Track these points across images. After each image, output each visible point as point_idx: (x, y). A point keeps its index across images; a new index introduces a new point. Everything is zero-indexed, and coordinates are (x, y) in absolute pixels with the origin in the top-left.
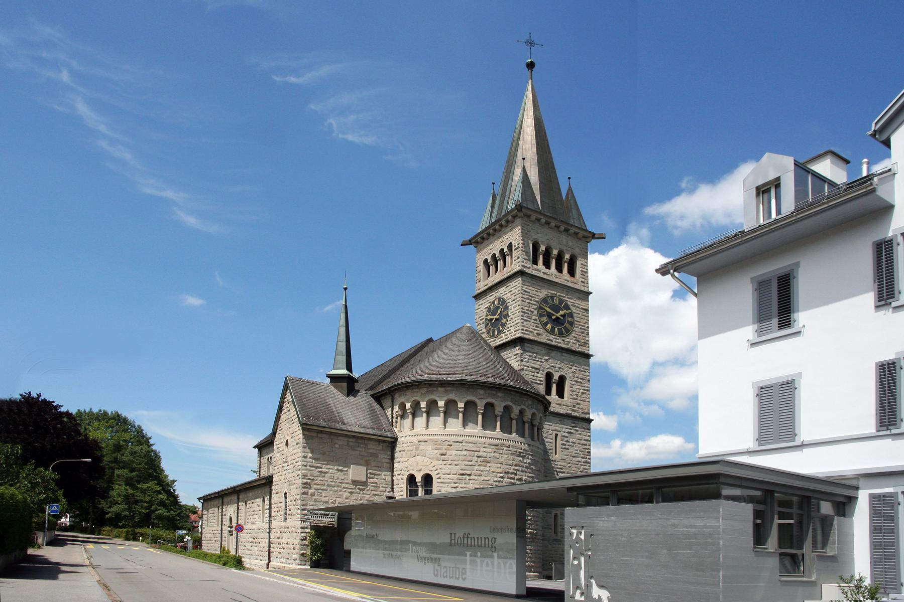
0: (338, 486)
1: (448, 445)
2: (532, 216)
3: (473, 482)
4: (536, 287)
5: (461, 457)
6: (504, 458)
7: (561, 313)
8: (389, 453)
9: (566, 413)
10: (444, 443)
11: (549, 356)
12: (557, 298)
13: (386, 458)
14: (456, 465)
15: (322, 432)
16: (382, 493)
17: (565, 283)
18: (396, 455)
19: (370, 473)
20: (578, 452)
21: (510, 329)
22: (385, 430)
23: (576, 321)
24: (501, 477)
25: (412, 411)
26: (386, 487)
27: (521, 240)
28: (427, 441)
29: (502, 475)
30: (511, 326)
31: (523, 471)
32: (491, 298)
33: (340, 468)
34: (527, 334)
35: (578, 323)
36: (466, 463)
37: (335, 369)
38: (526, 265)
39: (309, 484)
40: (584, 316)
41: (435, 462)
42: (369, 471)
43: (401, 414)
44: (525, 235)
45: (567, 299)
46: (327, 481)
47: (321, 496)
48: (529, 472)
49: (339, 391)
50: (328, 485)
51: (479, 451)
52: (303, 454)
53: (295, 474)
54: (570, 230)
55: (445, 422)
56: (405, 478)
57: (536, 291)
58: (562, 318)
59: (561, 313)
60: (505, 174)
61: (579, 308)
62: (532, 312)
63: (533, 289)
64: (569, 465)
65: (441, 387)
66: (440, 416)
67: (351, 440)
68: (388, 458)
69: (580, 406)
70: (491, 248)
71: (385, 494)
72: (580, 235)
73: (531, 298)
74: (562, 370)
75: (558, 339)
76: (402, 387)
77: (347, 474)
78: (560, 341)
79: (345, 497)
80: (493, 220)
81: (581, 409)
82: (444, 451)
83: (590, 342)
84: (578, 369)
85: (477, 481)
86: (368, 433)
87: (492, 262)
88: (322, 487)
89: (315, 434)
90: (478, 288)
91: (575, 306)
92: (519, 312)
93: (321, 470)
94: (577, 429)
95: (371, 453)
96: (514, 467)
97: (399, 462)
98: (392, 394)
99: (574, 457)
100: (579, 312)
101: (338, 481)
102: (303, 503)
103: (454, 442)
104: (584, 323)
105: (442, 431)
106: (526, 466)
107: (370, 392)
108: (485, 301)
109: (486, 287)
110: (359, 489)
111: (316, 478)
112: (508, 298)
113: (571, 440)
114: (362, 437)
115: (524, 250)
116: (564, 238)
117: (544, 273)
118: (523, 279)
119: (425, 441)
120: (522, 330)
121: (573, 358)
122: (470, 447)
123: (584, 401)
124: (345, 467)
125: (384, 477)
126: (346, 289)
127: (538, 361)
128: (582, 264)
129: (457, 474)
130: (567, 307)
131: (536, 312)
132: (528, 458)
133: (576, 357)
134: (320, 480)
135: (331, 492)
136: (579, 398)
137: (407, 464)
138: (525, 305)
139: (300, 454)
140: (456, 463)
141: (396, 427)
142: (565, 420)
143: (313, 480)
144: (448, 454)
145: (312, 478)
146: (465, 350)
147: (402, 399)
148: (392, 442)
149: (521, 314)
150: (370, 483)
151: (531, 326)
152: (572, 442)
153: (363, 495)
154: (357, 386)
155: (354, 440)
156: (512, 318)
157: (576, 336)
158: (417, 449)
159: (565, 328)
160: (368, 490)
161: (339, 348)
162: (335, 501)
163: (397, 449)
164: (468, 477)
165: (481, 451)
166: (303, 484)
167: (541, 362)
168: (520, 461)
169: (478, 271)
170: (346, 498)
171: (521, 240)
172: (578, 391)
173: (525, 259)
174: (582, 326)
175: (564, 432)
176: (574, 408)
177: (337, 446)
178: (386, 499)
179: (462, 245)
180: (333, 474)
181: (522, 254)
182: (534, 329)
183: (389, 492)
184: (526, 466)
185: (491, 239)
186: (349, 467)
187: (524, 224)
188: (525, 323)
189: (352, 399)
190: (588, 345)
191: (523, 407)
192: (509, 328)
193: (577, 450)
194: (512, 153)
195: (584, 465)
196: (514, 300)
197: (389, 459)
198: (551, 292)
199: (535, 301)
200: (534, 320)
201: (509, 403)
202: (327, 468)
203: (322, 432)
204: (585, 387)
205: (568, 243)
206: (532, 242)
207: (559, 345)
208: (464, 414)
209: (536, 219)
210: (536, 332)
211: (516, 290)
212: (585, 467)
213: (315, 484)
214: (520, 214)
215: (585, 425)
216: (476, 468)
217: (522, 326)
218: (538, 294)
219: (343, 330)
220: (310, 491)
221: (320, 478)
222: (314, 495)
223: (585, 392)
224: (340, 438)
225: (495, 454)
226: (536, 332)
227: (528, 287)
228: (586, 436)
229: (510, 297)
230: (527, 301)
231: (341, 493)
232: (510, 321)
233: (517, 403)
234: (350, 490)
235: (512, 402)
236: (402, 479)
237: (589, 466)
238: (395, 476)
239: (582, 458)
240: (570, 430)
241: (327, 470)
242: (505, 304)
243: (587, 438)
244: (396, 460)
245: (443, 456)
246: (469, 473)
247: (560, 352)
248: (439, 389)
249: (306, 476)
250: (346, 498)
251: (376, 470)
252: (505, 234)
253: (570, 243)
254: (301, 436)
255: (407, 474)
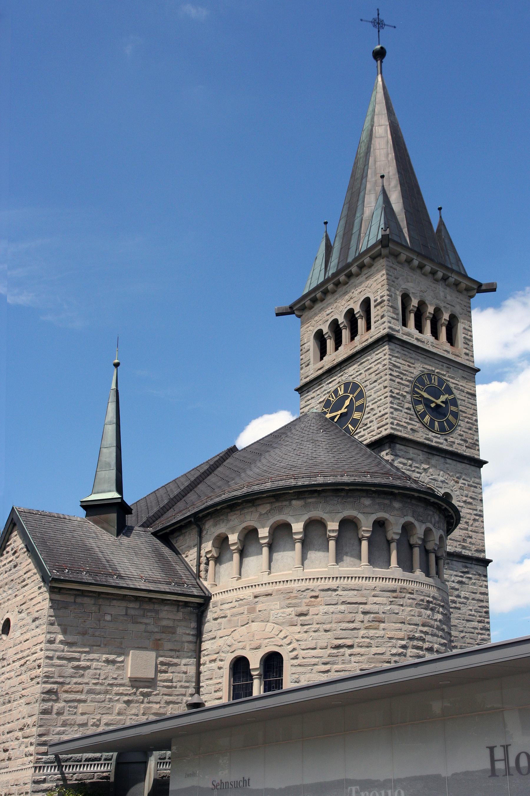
0: (106, 692)
1: (311, 597)
2: (402, 254)
3: (357, 658)
4: (408, 360)
5: (334, 616)
6: (406, 612)
7: (443, 398)
8: (194, 625)
9: (455, 552)
10: (304, 593)
11: (428, 464)
12: (436, 377)
13: (189, 634)
14: (326, 631)
15: (83, 593)
16: (180, 697)
17: (445, 355)
18: (207, 627)
19: (162, 664)
20: (473, 613)
21: (368, 426)
22: (188, 585)
23: (461, 411)
24: (404, 647)
25: (240, 547)
26: (187, 687)
27: (387, 290)
28: (271, 595)
29: (404, 643)
30: (371, 422)
31: (433, 635)
32: (330, 385)
33: (112, 657)
34: (398, 430)
35: (464, 415)
36: (345, 625)
37: (94, 493)
38: (394, 327)
39: (56, 693)
40: (470, 403)
41: (287, 630)
42: (161, 659)
43: (216, 555)
44: (391, 283)
45: (448, 379)
46: (87, 684)
47: (75, 713)
48: (441, 637)
49: (102, 528)
50: (90, 692)
51: (365, 604)
52: (49, 636)
53: (24, 677)
54: (450, 278)
55: (304, 558)
56: (226, 665)
57: (409, 366)
58: (444, 405)
59: (443, 398)
60: (346, 206)
61: (463, 392)
62: (404, 396)
63: (404, 362)
64: (462, 635)
65: (298, 499)
66: (293, 549)
67: (131, 605)
68: (192, 633)
69: (473, 540)
70: (328, 312)
71: (185, 699)
72: (463, 286)
73: (402, 376)
74: (446, 485)
75: (439, 438)
76: (221, 509)
77: (122, 668)
78: (441, 441)
79: (117, 711)
80: (332, 270)
81: (473, 544)
82: (303, 609)
83: (481, 443)
84: (466, 483)
85: (363, 657)
86: (163, 590)
87: (330, 334)
88: (78, 697)
89: (71, 599)
90: (305, 375)
91: (458, 389)
92: (386, 397)
93: (77, 663)
94: (470, 576)
95: (164, 626)
96: (421, 628)
97: (214, 638)
98: (199, 523)
99: (468, 621)
100: (464, 398)
101: (107, 682)
102: (42, 730)
103: (323, 590)
104: (471, 415)
105: (299, 574)
106: (437, 625)
107: (151, 529)
108: (318, 392)
109: (320, 372)
110: (142, 694)
111: (68, 680)
112: (365, 379)
113: (463, 594)
114: (151, 599)
115: (390, 304)
116: (441, 290)
117: (417, 339)
118: (391, 347)
119: (267, 595)
120: (392, 423)
121: (460, 466)
122: (351, 596)
123: (477, 532)
124: (119, 655)
125: (184, 668)
126: (117, 365)
127: (414, 471)
128: (464, 328)
129: (329, 647)
130: (449, 391)
131: (409, 397)
132: (438, 612)
133: (464, 465)
134: (76, 683)
135: (94, 704)
136: (470, 528)
137: (229, 640)
138: (395, 386)
139: (42, 638)
140: (327, 627)
141: (206, 579)
142: (454, 563)
143: (62, 684)
144: (311, 613)
145: (61, 680)
146: (324, 443)
147: (221, 529)
148: (200, 605)
149: (389, 399)
150: (161, 681)
151: (402, 417)
152: (465, 598)
153: (148, 705)
154: (130, 520)
155: (136, 605)
156: (372, 409)
157: (462, 433)
158: (251, 610)
159: (448, 421)
160: (156, 695)
161: (103, 459)
162: (99, 720)
163: (210, 615)
164: (348, 651)
165: (369, 603)
166: (43, 693)
167: (418, 473)
168: (429, 616)
169: (304, 350)
170: (119, 714)
171: (387, 290)
172: (468, 516)
173: (392, 318)
174: (469, 418)
175: (453, 582)
176: (464, 544)
177: (108, 618)
178: (186, 708)
179: (278, 315)
180: (100, 669)
181: (388, 311)
182: (407, 423)
183: (192, 695)
184: (437, 625)
185: (330, 299)
186: (128, 655)
187: (391, 267)
188: (396, 413)
189: (124, 540)
190: (477, 447)
191: (430, 525)
192: (366, 424)
193: (471, 610)
194: (358, 175)
195: (482, 634)
196: (375, 381)
197: (193, 635)
198: (428, 367)
199: (408, 381)
200: (407, 409)
201: (410, 519)
202: (88, 660)
203: (83, 593)
204: (476, 510)
205: (446, 298)
206: (401, 294)
207: (440, 446)
208: (338, 540)
209: (406, 261)
210: (410, 427)
211: (380, 366)
212: (483, 636)
213: (66, 692)
214: (385, 251)
215: (480, 569)
216: (362, 632)
217: (392, 418)
218: (411, 370)
219: (111, 430)
220: (57, 706)
221: (75, 680)
222: (63, 713)
223: (477, 518)
224: (115, 602)
225: (392, 606)
226: (410, 427)
227: (398, 360)
228: (481, 586)
229: (368, 377)
230: (398, 380)
231: (111, 704)
232: (369, 413)
233: (421, 518)
234: (126, 698)
235: (413, 517)
236: (220, 668)
237: (489, 635)
238: (204, 664)
239: (479, 622)
240: (460, 579)
241: (88, 663)
242: (359, 389)
243: (483, 590)
244: (205, 636)
245: (302, 618)
246: (350, 644)
247: (442, 457)
248: (294, 502)
249: (52, 677)
250: (119, 714)
251: (171, 657)
252: (356, 287)
253: (449, 298)
254: (47, 604)
255: (230, 657)
